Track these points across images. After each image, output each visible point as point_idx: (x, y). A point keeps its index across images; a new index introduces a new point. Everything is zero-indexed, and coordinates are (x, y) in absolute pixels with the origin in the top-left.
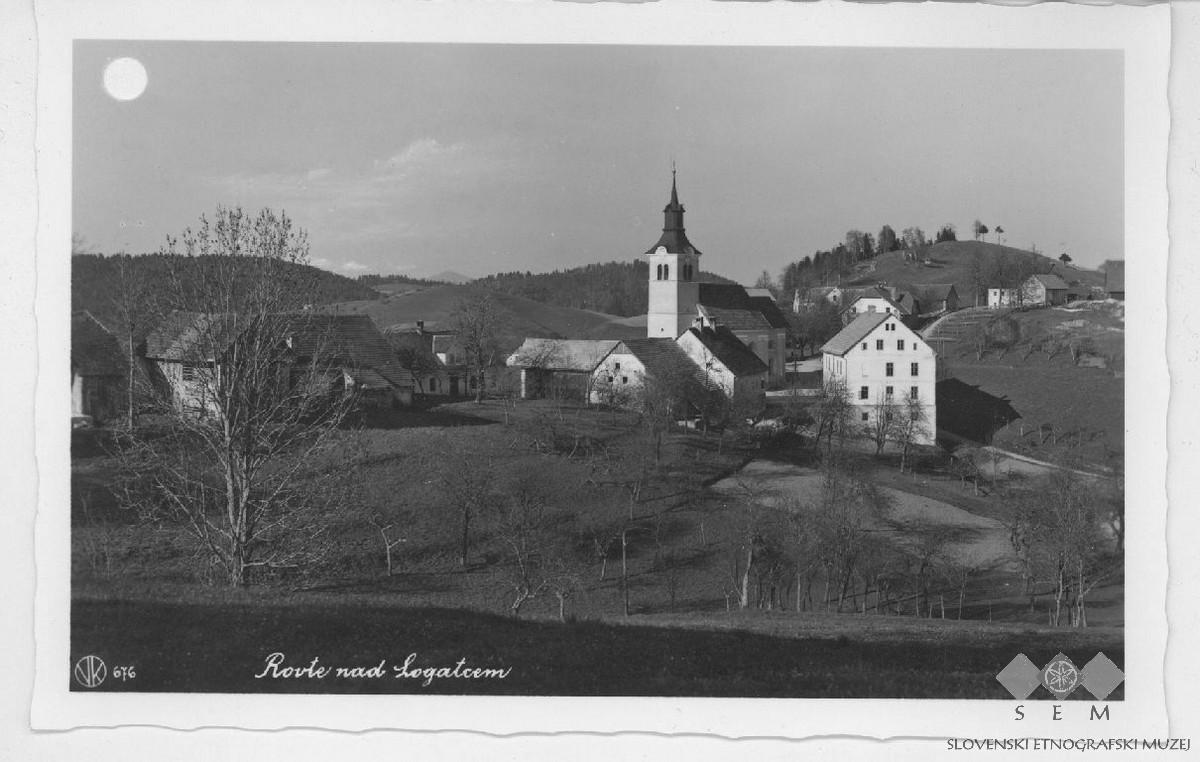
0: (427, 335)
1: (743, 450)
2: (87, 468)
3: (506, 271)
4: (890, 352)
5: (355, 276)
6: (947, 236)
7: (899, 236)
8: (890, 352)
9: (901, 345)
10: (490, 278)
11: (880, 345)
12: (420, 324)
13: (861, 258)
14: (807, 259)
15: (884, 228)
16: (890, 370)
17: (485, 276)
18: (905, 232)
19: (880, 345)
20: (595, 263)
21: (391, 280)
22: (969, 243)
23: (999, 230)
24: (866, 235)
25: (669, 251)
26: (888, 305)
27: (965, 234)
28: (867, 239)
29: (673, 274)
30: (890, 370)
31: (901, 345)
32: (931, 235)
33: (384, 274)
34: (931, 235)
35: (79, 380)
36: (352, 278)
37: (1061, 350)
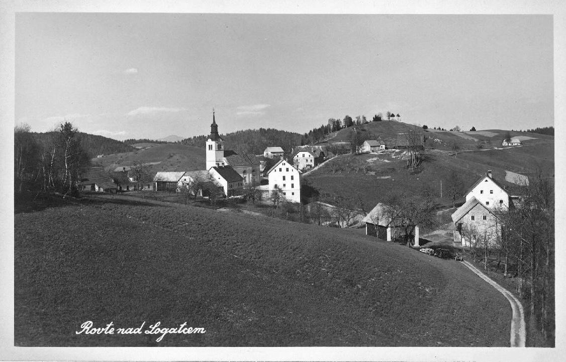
0: (126, 172)
1: (168, 201)
2: (20, 291)
3: (197, 135)
4: (284, 172)
5: (122, 139)
6: (377, 119)
7: (354, 119)
8: (284, 172)
9: (287, 170)
10: (190, 139)
11: (280, 170)
12: (124, 168)
13: (334, 130)
14: (311, 131)
15: (346, 116)
16: (284, 178)
17: (187, 138)
18: (357, 118)
19: (280, 170)
20: (240, 130)
21: (141, 141)
22: (386, 121)
23: (398, 116)
24: (338, 121)
25: (212, 140)
26: (309, 154)
27: (385, 118)
28: (338, 122)
29: (214, 148)
30: (284, 178)
31: (287, 170)
32: (370, 119)
33: (137, 139)
34: (370, 119)
35: (491, 135)
36: (121, 141)
37: (361, 170)
